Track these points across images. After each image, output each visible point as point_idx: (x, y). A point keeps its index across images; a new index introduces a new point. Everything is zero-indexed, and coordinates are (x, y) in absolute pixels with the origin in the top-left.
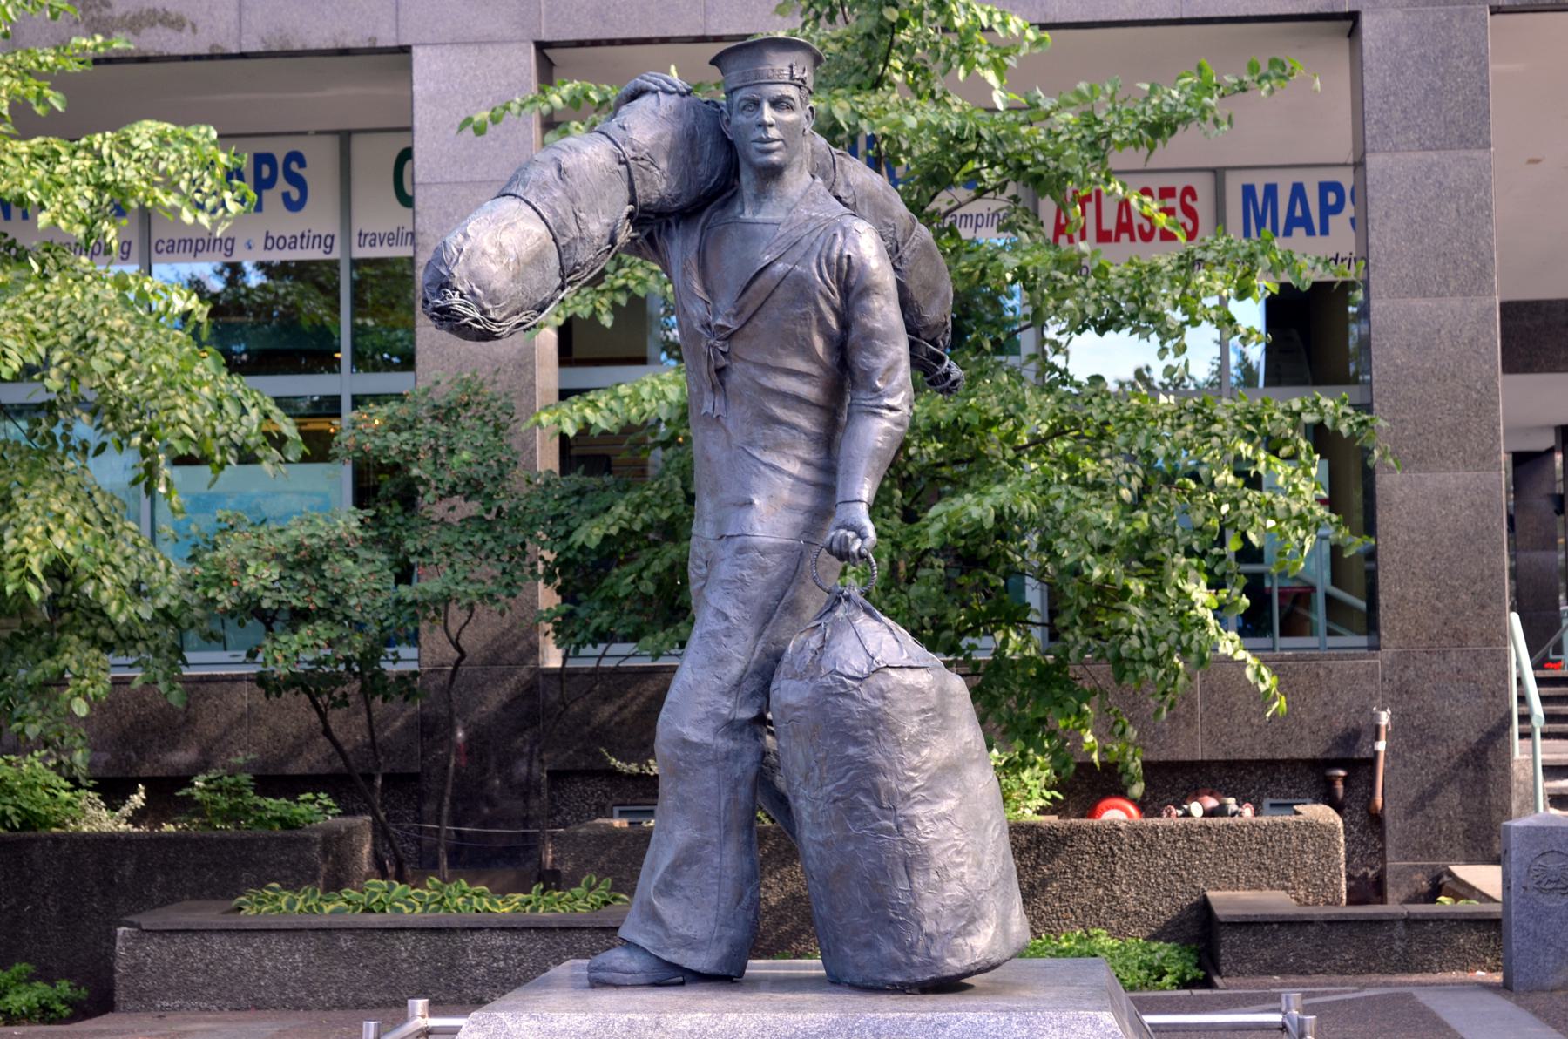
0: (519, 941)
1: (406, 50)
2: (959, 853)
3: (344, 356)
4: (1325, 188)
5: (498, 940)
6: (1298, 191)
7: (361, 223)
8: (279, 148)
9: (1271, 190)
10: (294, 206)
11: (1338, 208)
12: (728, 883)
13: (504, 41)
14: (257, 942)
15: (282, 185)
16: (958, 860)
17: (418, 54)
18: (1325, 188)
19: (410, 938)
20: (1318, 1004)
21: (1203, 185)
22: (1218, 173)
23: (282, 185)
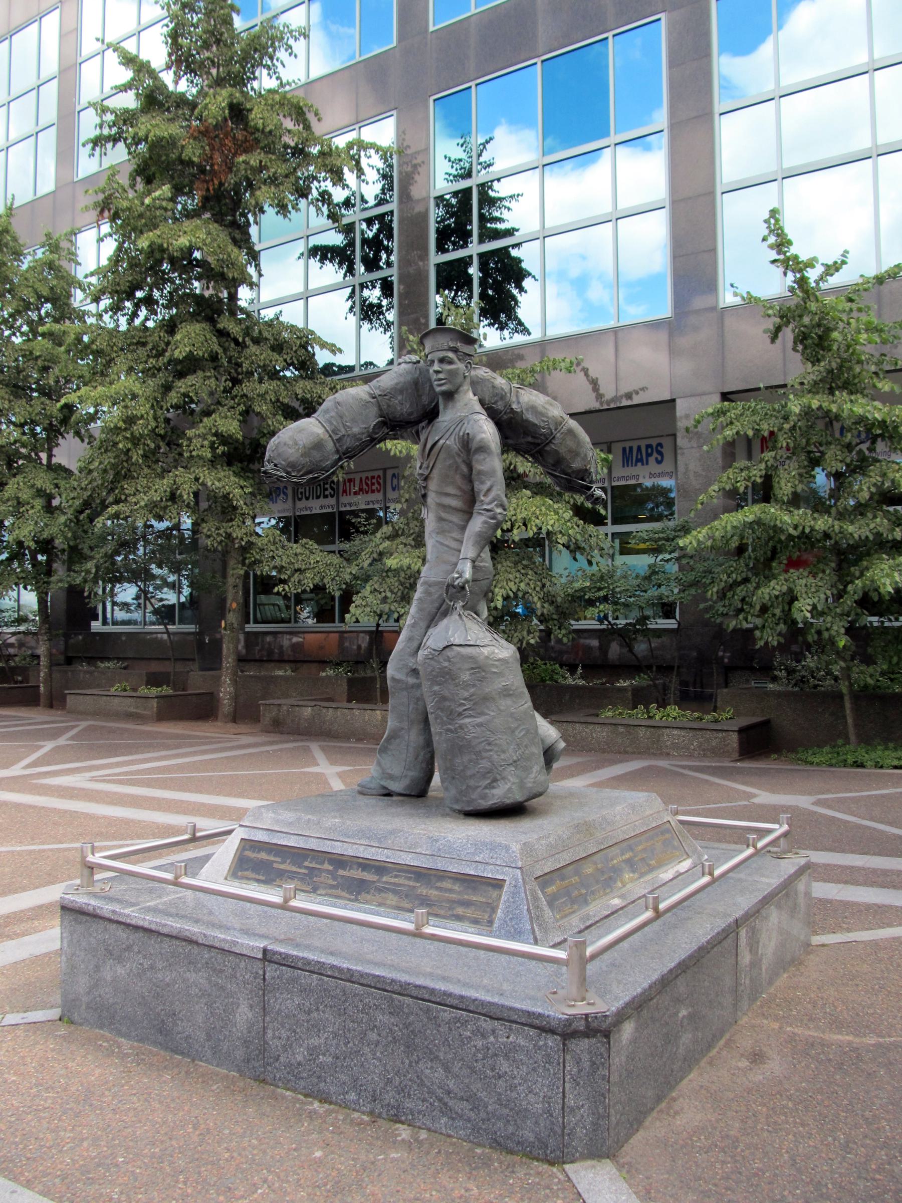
0: (683, 733)
1: (673, 400)
2: (489, 744)
3: (609, 521)
4: (648, 446)
5: (675, 732)
6: (639, 448)
7: (615, 474)
8: (654, 442)
9: (631, 448)
10: (659, 462)
11: (651, 455)
12: (411, 750)
13: (710, 393)
14: (591, 727)
15: (655, 455)
16: (488, 748)
17: (678, 401)
18: (648, 446)
19: (644, 729)
20: (827, 799)
21: (381, 473)
22: (385, 470)
23: (655, 455)
